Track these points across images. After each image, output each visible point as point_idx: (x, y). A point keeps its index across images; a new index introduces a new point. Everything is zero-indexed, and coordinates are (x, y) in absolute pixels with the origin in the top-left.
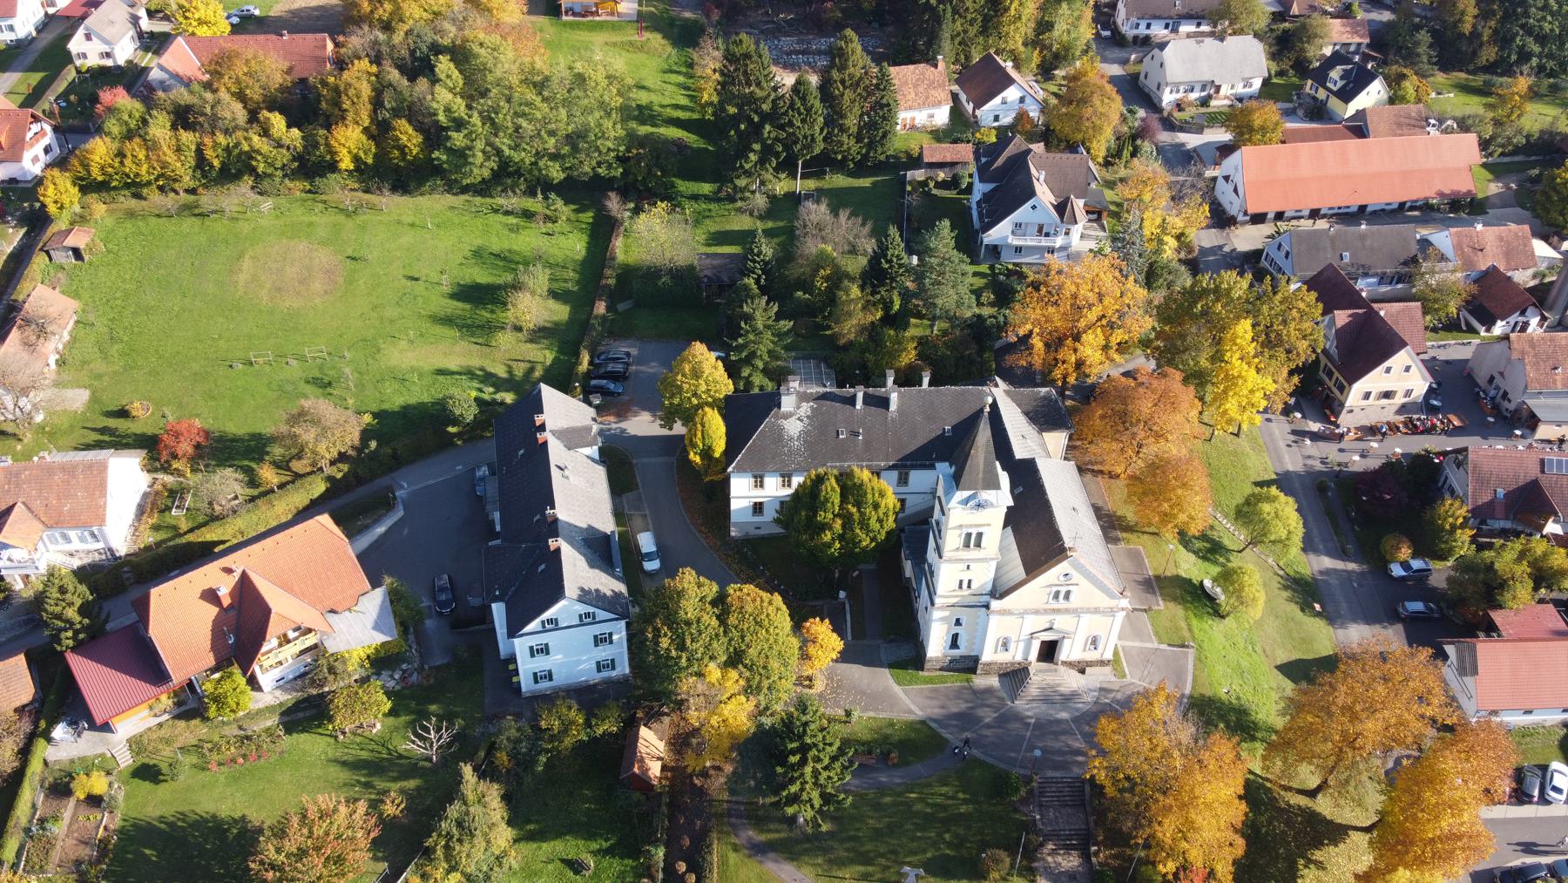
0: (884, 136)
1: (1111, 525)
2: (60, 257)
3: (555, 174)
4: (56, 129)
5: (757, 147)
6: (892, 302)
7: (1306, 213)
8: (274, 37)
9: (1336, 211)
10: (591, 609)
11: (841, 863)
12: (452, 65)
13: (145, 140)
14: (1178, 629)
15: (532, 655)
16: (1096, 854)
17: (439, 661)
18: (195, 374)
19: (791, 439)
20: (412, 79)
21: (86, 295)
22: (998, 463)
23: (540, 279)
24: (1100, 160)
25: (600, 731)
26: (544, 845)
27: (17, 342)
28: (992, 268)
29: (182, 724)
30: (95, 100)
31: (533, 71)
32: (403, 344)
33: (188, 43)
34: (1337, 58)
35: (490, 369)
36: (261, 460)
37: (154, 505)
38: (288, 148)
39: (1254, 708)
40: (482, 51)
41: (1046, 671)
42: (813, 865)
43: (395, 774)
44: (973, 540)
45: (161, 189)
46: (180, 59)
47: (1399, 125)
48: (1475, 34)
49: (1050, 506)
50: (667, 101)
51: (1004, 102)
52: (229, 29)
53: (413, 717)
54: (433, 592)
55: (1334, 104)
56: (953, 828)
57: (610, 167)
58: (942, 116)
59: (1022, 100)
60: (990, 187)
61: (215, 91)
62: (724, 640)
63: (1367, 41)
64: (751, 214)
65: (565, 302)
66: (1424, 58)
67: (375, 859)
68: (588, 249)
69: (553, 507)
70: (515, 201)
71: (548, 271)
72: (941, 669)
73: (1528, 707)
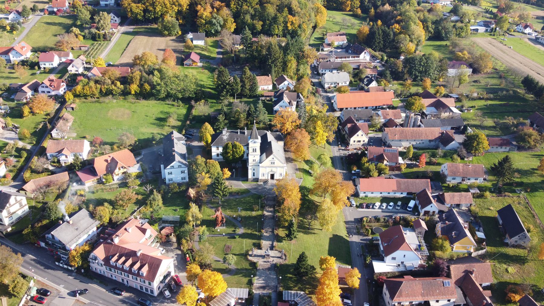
20: (149, 75)
23: (175, 116)
25: (181, 189)
34: (367, 77)
44: (254, 150)
45: (91, 97)
46: (95, 71)
51: (284, 84)
58: (270, 87)
59: (288, 84)
60: (276, 99)
63: (377, 74)
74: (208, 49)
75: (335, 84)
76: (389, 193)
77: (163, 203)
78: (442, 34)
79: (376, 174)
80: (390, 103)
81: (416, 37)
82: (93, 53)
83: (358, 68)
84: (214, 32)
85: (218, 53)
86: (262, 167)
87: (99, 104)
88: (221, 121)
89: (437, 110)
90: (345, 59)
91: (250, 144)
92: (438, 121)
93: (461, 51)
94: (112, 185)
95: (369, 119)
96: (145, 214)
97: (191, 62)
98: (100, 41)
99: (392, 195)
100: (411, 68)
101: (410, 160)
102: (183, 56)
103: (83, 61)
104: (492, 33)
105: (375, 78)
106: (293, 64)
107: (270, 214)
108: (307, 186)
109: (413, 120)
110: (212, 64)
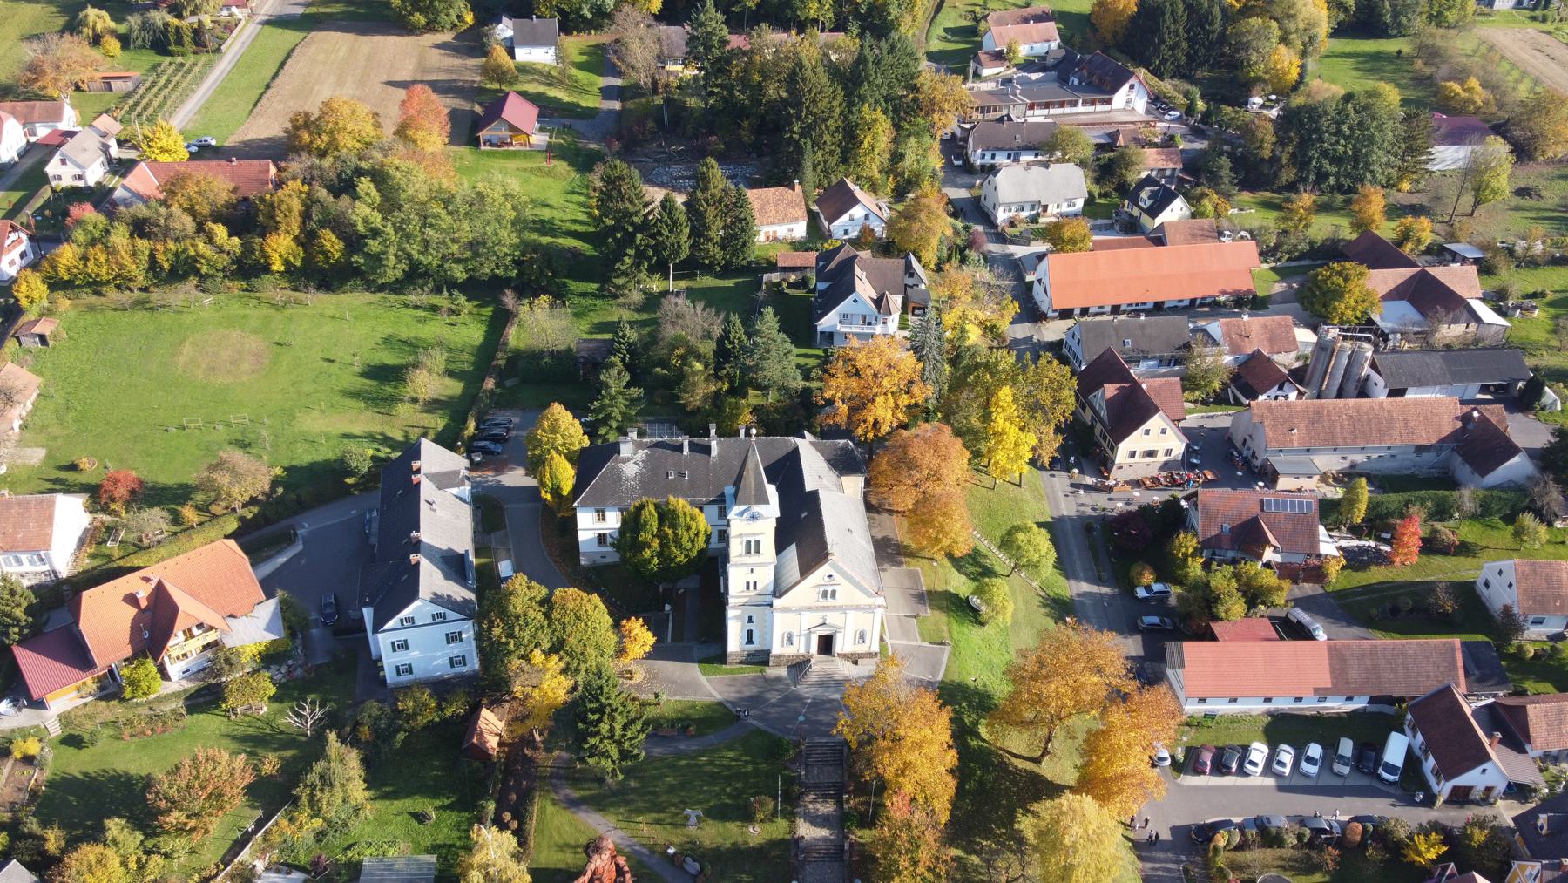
0: (744, 244)
1: (887, 551)
2: (28, 342)
3: (459, 275)
4: (31, 238)
5: (631, 252)
7: (1108, 309)
8: (223, 163)
9: (1134, 308)
10: (442, 610)
11: (639, 812)
12: (372, 185)
13: (107, 247)
15: (394, 650)
16: (848, 801)
17: (321, 660)
19: (628, 479)
20: (336, 196)
23: (439, 360)
24: (932, 266)
25: (448, 713)
26: (396, 803)
28: (826, 351)
29: (103, 704)
30: (66, 214)
31: (440, 190)
32: (316, 413)
33: (149, 167)
34: (1149, 181)
35: (389, 434)
36: (183, 504)
37: (93, 538)
38: (229, 253)
40: (398, 174)
42: (617, 814)
44: (753, 548)
45: (118, 287)
46: (143, 180)
47: (1194, 236)
48: (1274, 160)
50: (568, 217)
51: (852, 219)
52: (187, 156)
55: (1145, 219)
57: (506, 268)
58: (800, 230)
59: (867, 217)
61: (168, 207)
63: (1180, 166)
66: (1226, 180)
67: (253, 807)
68: (486, 337)
70: (425, 298)
71: (446, 355)
72: (740, 663)
73: (1233, 695)
74: (570, 77)
75: (1032, 208)
76: (1299, 699)
77: (372, 781)
78: (1381, 15)
79: (1237, 607)
80: (1243, 284)
81: (1301, 26)
82: (151, 101)
83: (1109, 144)
84: (589, 16)
85: (607, 93)
86: (785, 610)
87: (147, 314)
88: (613, 391)
89: (1423, 314)
90: (1060, 111)
91: (732, 523)
92: (1436, 362)
93: (1460, 75)
94: (159, 700)
95: (1179, 357)
96: (288, 847)
97: (505, 133)
98: (183, 55)
99: (1310, 706)
100: (1305, 143)
101: (1356, 531)
102: (478, 109)
103: (104, 135)
104: (1538, 13)
105: (1175, 180)
106: (879, 135)
107: (824, 833)
108: (970, 680)
109: (1345, 361)
110: (583, 136)
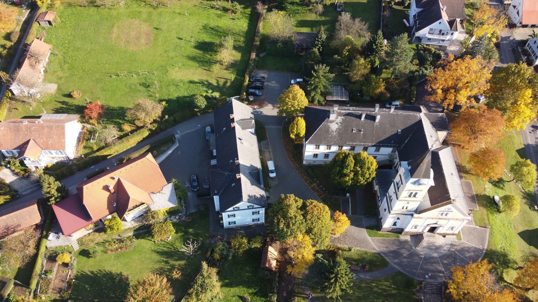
6: (375, 62)
14: (484, 219)
17: (193, 211)
18: (97, 79)
19: (333, 131)
21: (54, 41)
22: (432, 170)
23: (230, 42)
25: (253, 247)
26: (232, 289)
27: (28, 64)
28: (417, 46)
29: (97, 234)
32: (177, 69)
35: (210, 81)
39: (509, 253)
41: (430, 236)
43: (177, 258)
49: (444, 177)
53: (183, 234)
54: (191, 182)
56: (389, 299)
60: (420, 10)
62: (305, 224)
64: (316, 13)
65: (239, 52)
68: (249, 26)
69: (238, 159)
72: (388, 231)
